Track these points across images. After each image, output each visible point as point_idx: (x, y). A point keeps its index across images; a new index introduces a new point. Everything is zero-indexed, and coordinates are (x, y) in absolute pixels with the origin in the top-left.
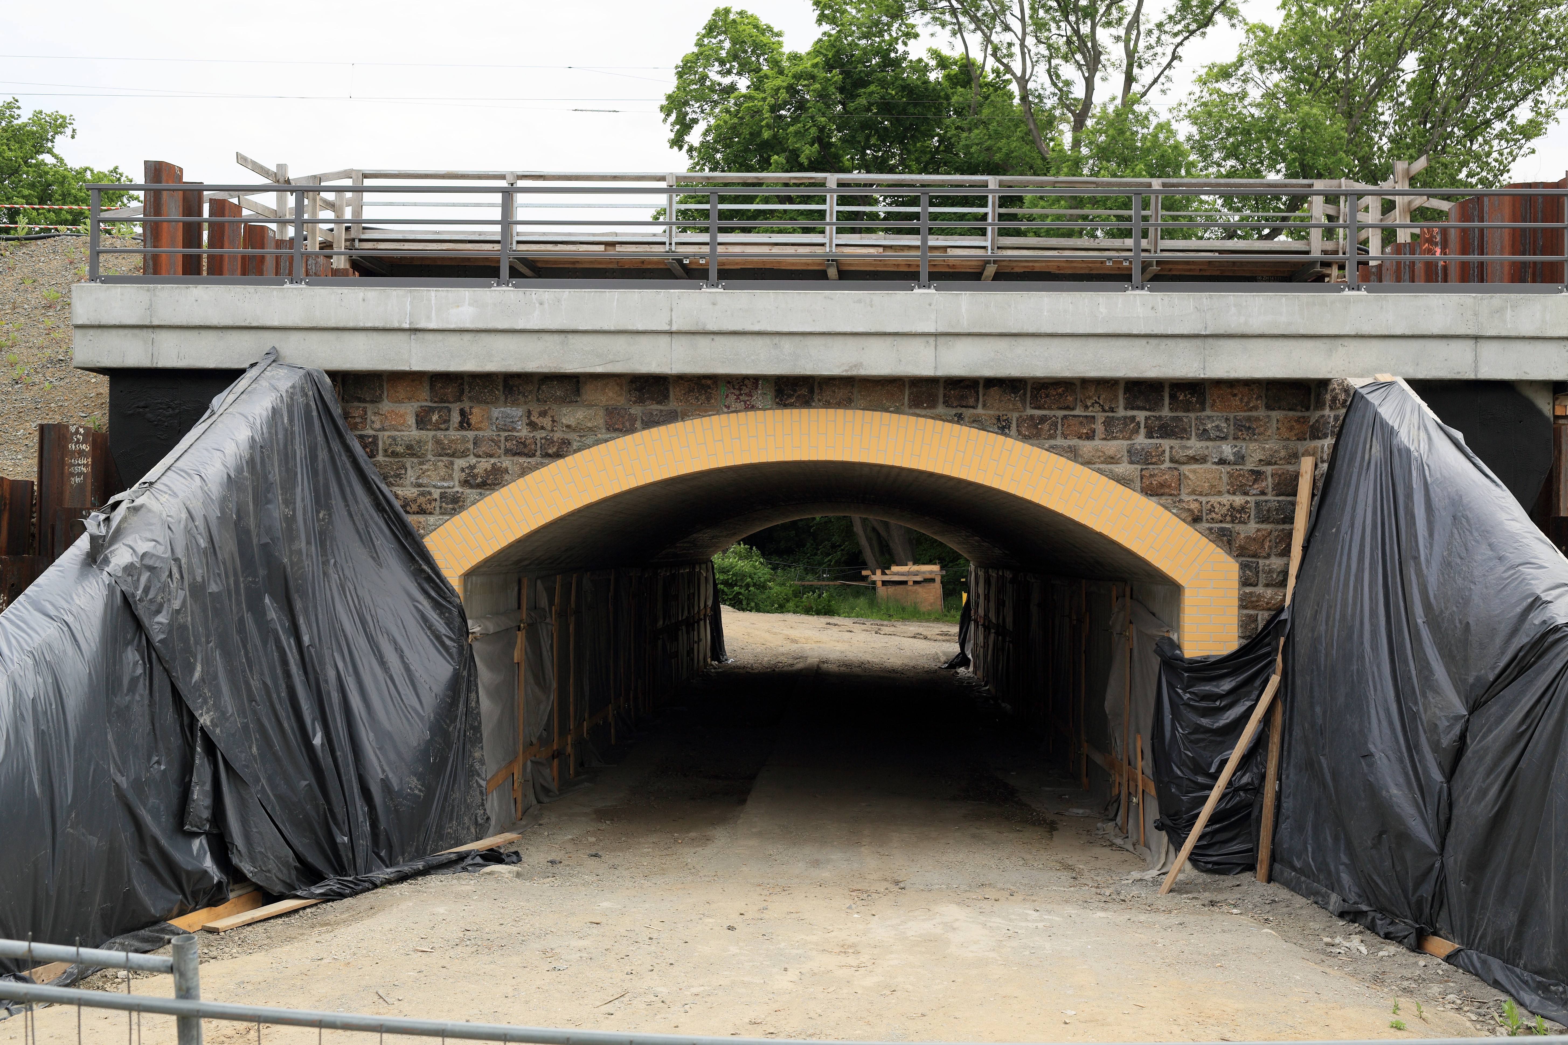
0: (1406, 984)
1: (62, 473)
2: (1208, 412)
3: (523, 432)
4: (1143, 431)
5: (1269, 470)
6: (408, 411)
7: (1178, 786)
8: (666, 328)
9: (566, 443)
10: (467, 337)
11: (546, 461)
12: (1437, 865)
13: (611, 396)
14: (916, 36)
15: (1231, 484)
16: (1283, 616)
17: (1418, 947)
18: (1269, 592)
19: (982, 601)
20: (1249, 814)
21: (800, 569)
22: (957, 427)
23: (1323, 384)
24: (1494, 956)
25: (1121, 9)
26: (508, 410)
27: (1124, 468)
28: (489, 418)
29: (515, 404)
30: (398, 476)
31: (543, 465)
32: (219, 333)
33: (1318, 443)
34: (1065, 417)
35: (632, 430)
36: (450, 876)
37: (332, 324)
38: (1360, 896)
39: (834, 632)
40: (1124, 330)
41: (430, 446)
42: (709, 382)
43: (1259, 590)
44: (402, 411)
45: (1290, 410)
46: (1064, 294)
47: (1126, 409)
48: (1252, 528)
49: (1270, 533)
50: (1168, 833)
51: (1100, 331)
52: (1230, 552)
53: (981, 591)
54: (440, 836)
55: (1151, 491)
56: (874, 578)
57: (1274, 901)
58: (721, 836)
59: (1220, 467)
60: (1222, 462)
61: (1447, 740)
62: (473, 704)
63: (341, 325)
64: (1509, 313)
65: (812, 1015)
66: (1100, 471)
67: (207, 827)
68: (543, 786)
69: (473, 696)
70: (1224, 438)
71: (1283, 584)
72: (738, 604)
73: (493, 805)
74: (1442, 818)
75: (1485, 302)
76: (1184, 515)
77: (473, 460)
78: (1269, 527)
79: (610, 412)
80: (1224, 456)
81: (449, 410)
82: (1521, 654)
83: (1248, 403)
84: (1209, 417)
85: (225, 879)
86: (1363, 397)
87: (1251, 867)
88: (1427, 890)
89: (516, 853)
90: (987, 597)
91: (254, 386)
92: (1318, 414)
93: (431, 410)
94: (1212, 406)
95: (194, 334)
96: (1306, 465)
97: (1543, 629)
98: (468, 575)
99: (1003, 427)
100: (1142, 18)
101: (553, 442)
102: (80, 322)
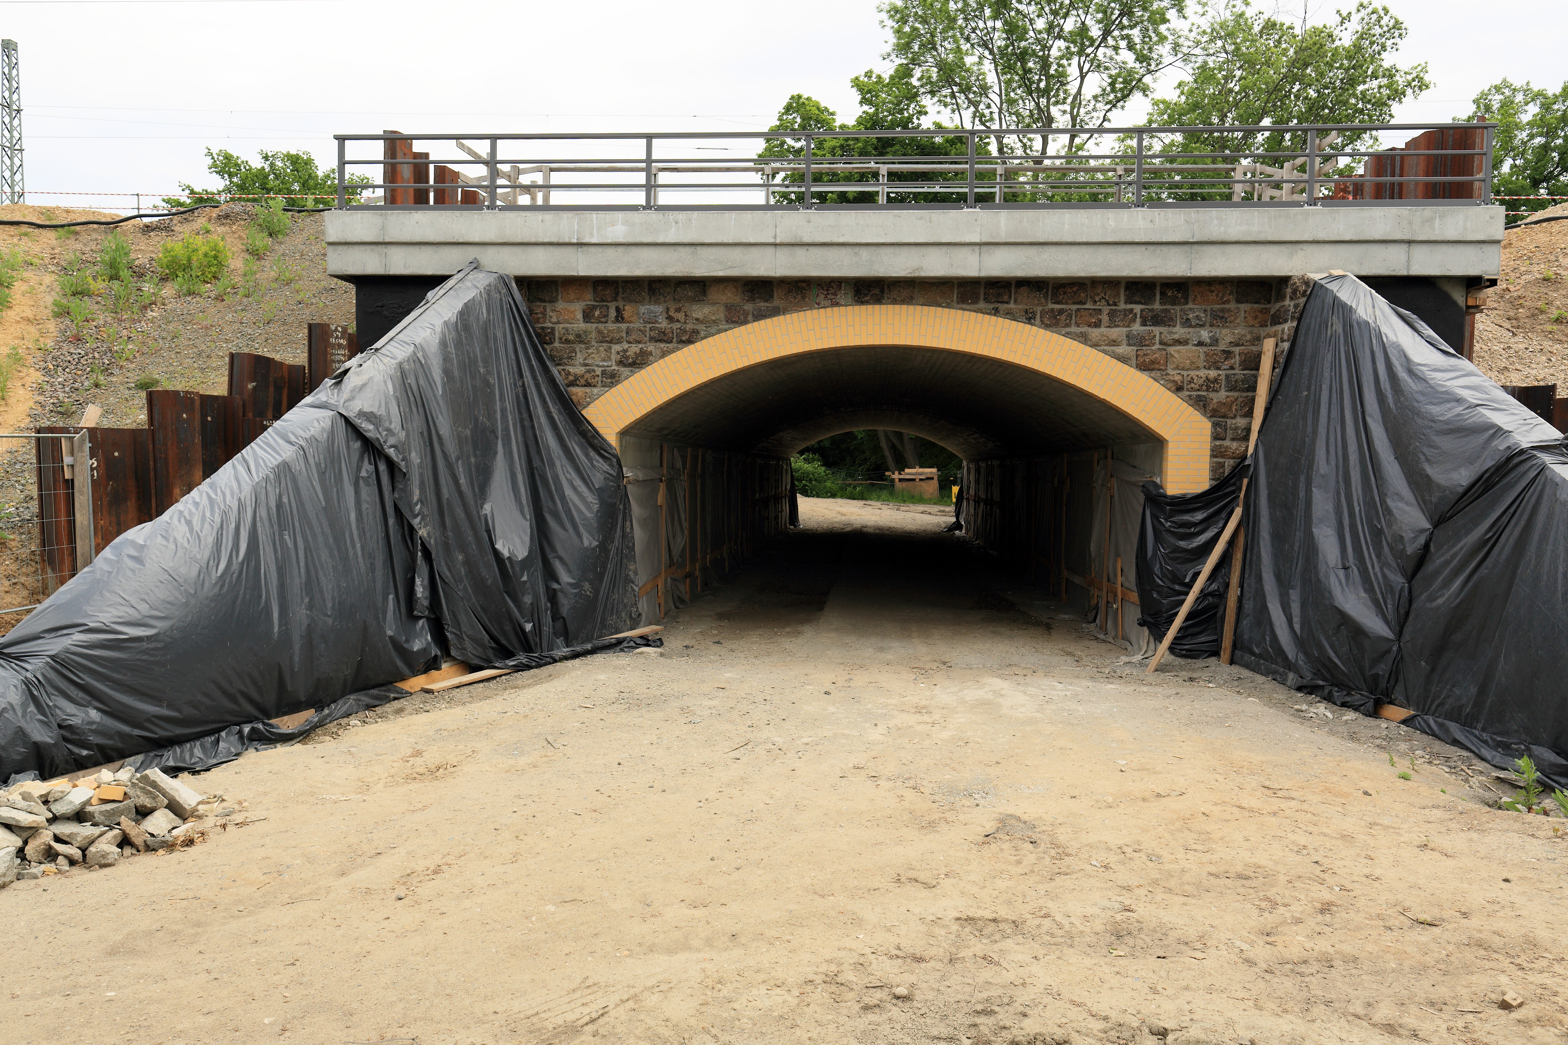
0: (1378, 742)
1: (326, 360)
2: (1190, 306)
3: (664, 324)
4: (1138, 320)
5: (1237, 350)
6: (577, 309)
7: (1159, 592)
8: (772, 241)
9: (695, 332)
10: (621, 249)
12: (1395, 648)
13: (729, 296)
14: (926, 113)
15: (1207, 361)
16: (1247, 463)
17: (1375, 713)
18: (1235, 445)
19: (972, 484)
20: (1215, 614)
21: (843, 474)
22: (994, 318)
23: (1284, 281)
24: (1451, 720)
25: (1065, 92)
26: (652, 307)
27: (1123, 349)
28: (638, 314)
29: (657, 302)
30: (570, 358)
31: (678, 349)
32: (434, 248)
33: (1279, 328)
34: (1078, 310)
35: (745, 322)
36: (611, 655)
37: (518, 240)
38: (1315, 674)
39: (869, 509)
40: (1128, 239)
41: (593, 335)
42: (804, 285)
43: (1227, 443)
44: (573, 309)
45: (1256, 303)
46: (1082, 211)
47: (1126, 303)
48: (1222, 395)
49: (1237, 399)
50: (1149, 628)
51: (1109, 240)
52: (1204, 414)
53: (972, 478)
54: (604, 626)
55: (1144, 367)
56: (893, 476)
57: (1240, 678)
58: (808, 631)
60: (1200, 344)
61: (1411, 549)
62: (628, 530)
63: (526, 240)
64: (1437, 222)
65: (904, 761)
66: (1105, 352)
67: (427, 613)
68: (679, 597)
69: (628, 523)
71: (1246, 438)
72: (806, 494)
73: (643, 605)
74: (1402, 611)
75: (1418, 213)
76: (1169, 385)
77: (626, 346)
78: (1236, 394)
79: (729, 308)
80: (1202, 339)
81: (608, 308)
82: (1486, 476)
83: (1222, 297)
84: (1191, 309)
85: (439, 653)
86: (1322, 286)
87: (1216, 653)
88: (1383, 669)
89: (660, 640)
90: (977, 482)
91: (459, 285)
92: (1278, 305)
93: (594, 308)
94: (1194, 300)
95: (417, 248)
96: (1269, 345)
97: (1507, 454)
98: (624, 434)
99: (1029, 319)
100: (1083, 92)
101: (685, 331)
102: (331, 240)
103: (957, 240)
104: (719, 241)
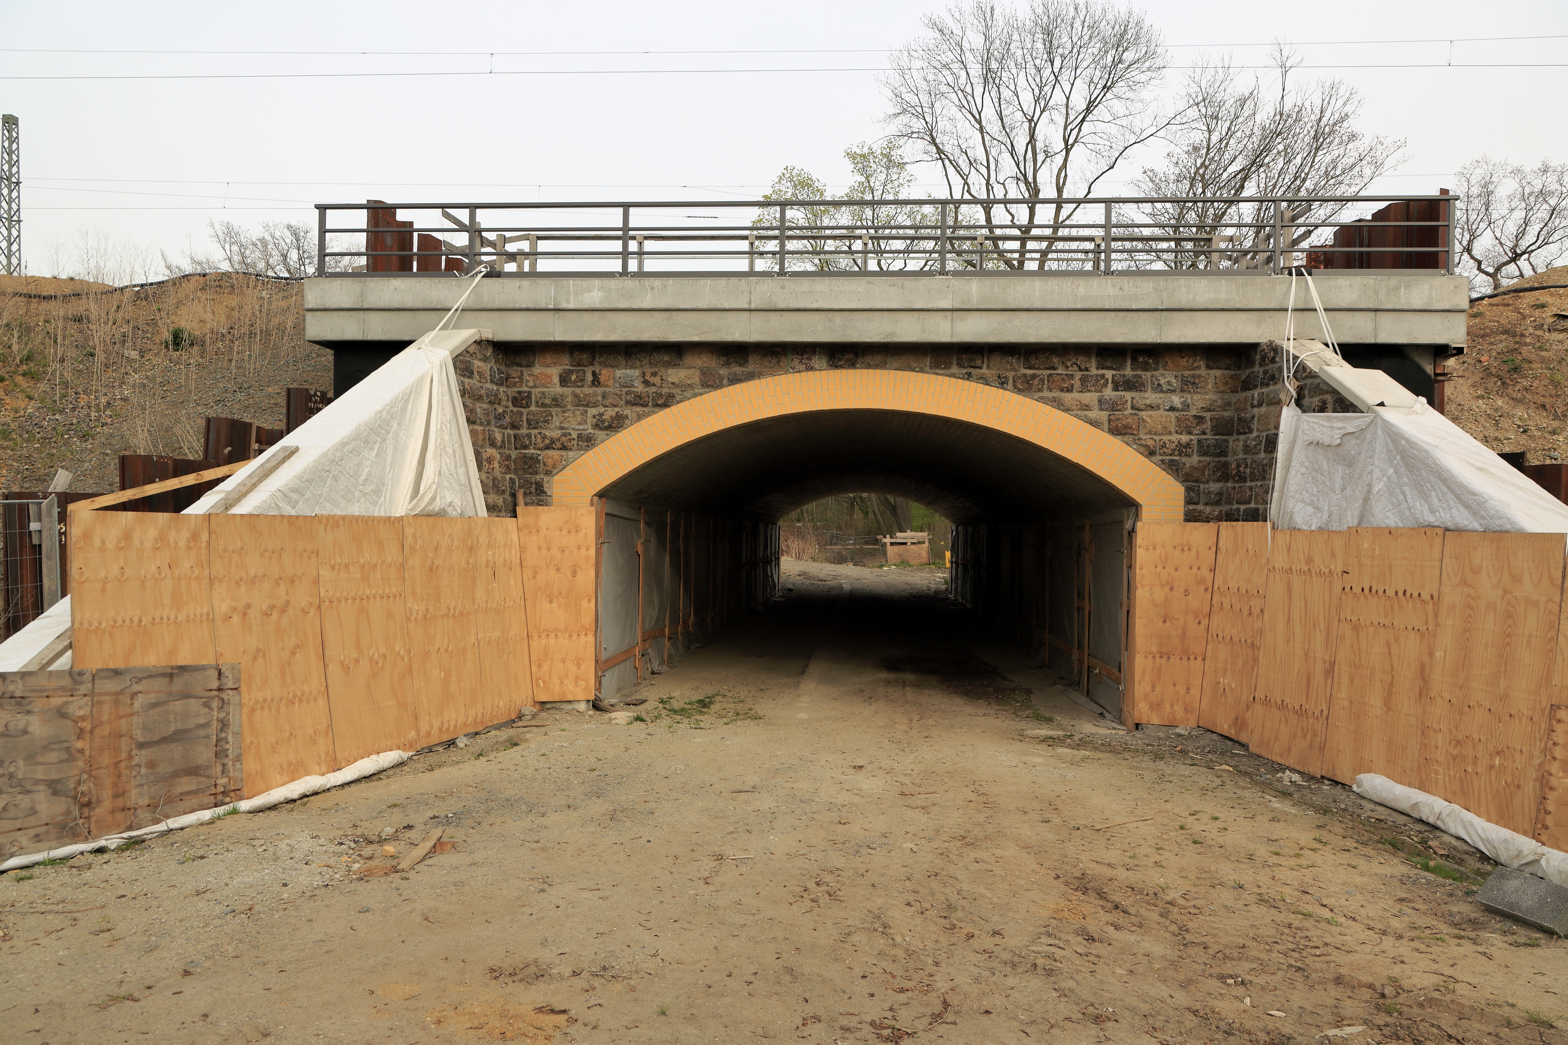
3: (639, 388)
4: (1110, 385)
5: (1208, 415)
8: (747, 306)
30: (547, 421)
31: (654, 413)
35: (720, 386)
43: (1201, 507)
51: (1079, 306)
60: (1172, 409)
78: (1208, 459)
93: (570, 372)
103: (930, 306)
104: (694, 306)
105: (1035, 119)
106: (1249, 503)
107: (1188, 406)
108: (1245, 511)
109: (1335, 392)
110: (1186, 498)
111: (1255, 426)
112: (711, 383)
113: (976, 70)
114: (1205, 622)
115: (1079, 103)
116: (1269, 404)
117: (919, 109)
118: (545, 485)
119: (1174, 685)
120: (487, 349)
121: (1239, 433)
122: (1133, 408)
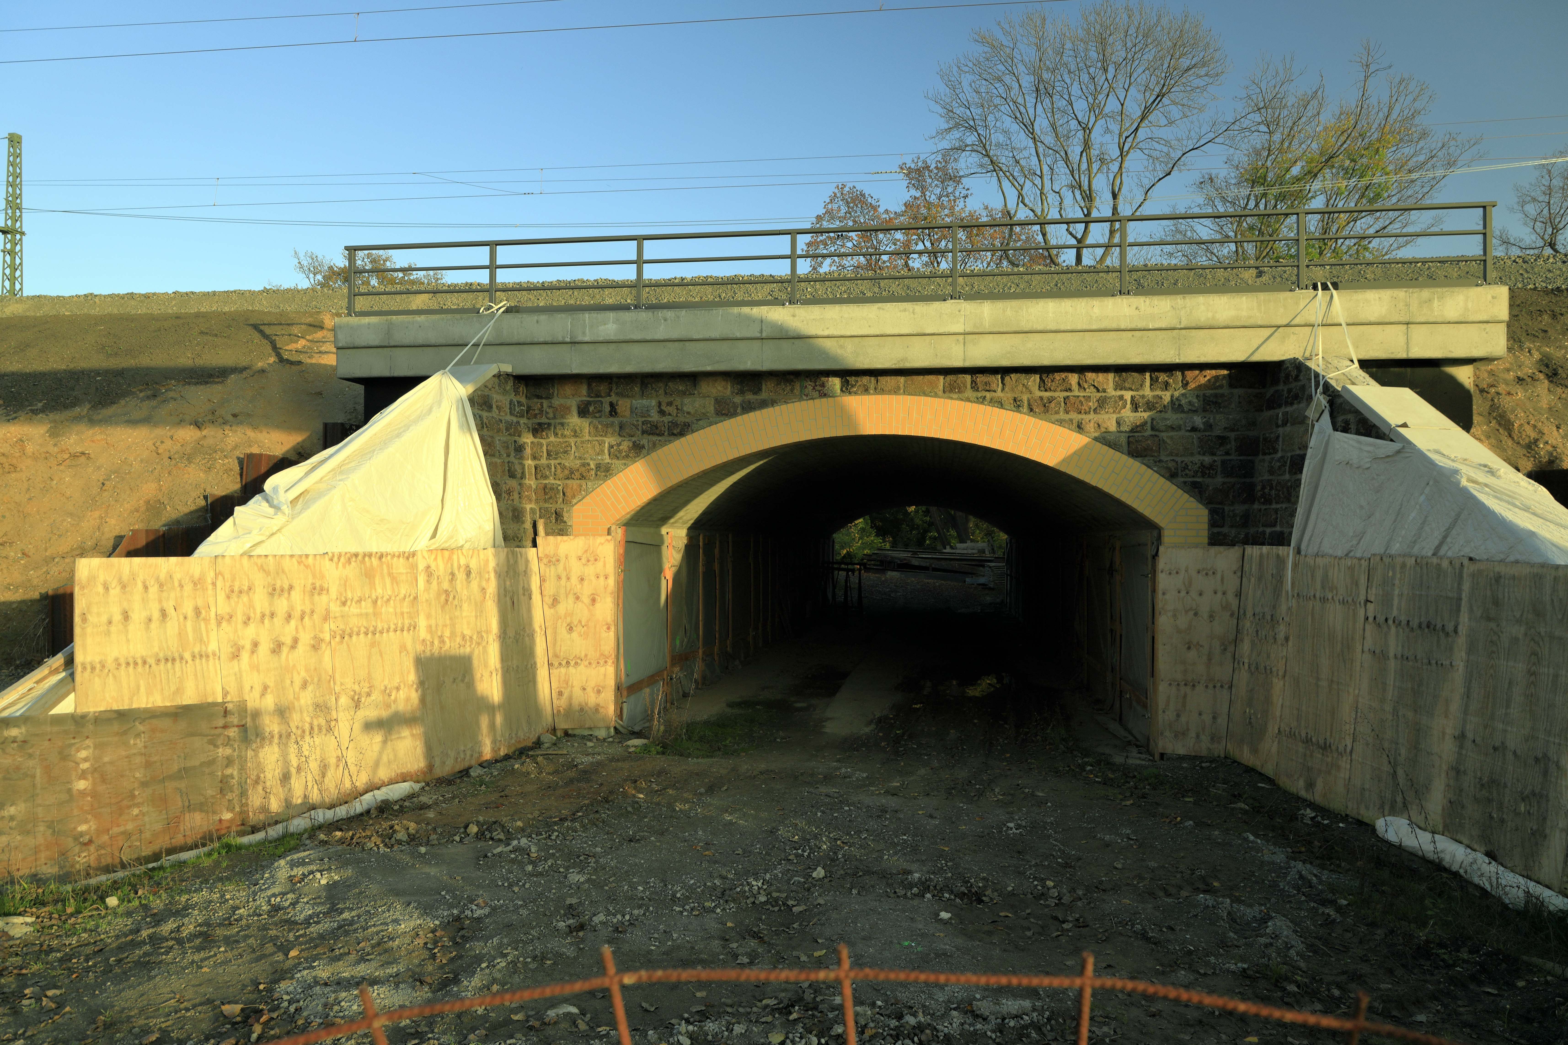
3: (655, 417)
4: (1129, 406)
5: (1232, 435)
8: (759, 335)
11: (672, 438)
13: (722, 389)
30: (566, 452)
31: (670, 442)
35: (734, 414)
43: (1225, 530)
51: (1094, 327)
59: (1192, 434)
60: (1194, 429)
63: (522, 341)
64: (1436, 303)
70: (1195, 411)
78: (1232, 480)
93: (589, 403)
103: (941, 331)
104: (707, 336)
105: (1090, 126)
106: (1275, 525)
107: (1211, 426)
108: (1271, 534)
109: (1357, 412)
110: (1209, 520)
111: (1280, 446)
112: (725, 411)
113: (1027, 81)
114: (1231, 648)
115: (1134, 110)
116: (1292, 424)
117: (972, 123)
118: (565, 515)
119: (1200, 714)
120: (506, 382)
121: (1264, 454)
122: (1153, 429)
